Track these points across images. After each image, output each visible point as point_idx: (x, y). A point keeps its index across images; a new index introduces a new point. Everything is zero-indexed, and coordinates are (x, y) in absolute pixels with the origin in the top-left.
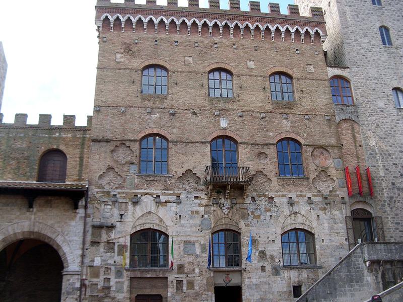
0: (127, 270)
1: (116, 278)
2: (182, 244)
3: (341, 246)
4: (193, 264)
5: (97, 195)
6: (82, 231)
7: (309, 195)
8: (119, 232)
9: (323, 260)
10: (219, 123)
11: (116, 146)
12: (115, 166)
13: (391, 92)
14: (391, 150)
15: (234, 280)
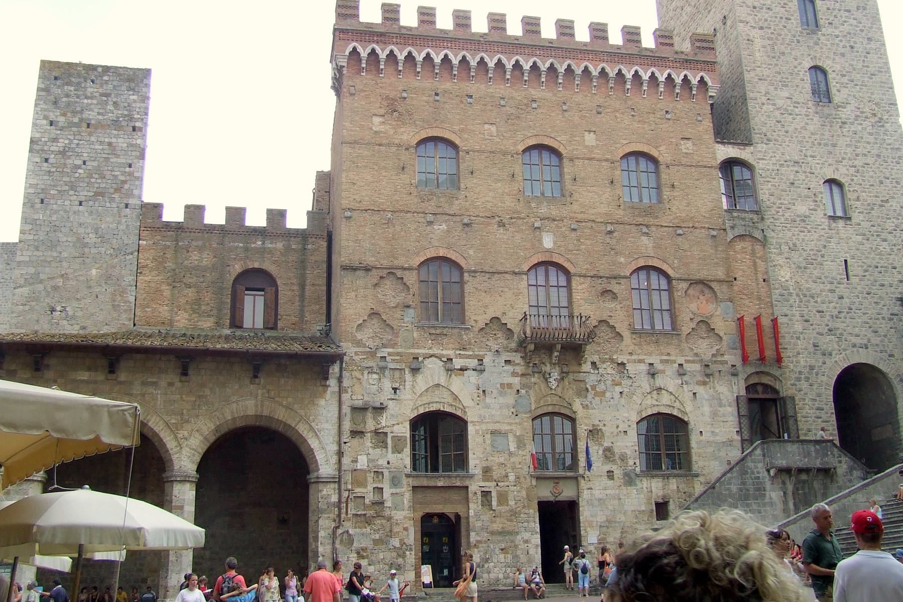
0: (408, 476)
1: (391, 488)
2: (488, 436)
3: (730, 442)
4: (505, 466)
5: (356, 358)
6: (337, 415)
7: (681, 360)
8: (392, 415)
9: (701, 463)
10: (540, 241)
11: (381, 277)
12: (381, 311)
13: (825, 189)
14: (816, 288)
15: (567, 493)
